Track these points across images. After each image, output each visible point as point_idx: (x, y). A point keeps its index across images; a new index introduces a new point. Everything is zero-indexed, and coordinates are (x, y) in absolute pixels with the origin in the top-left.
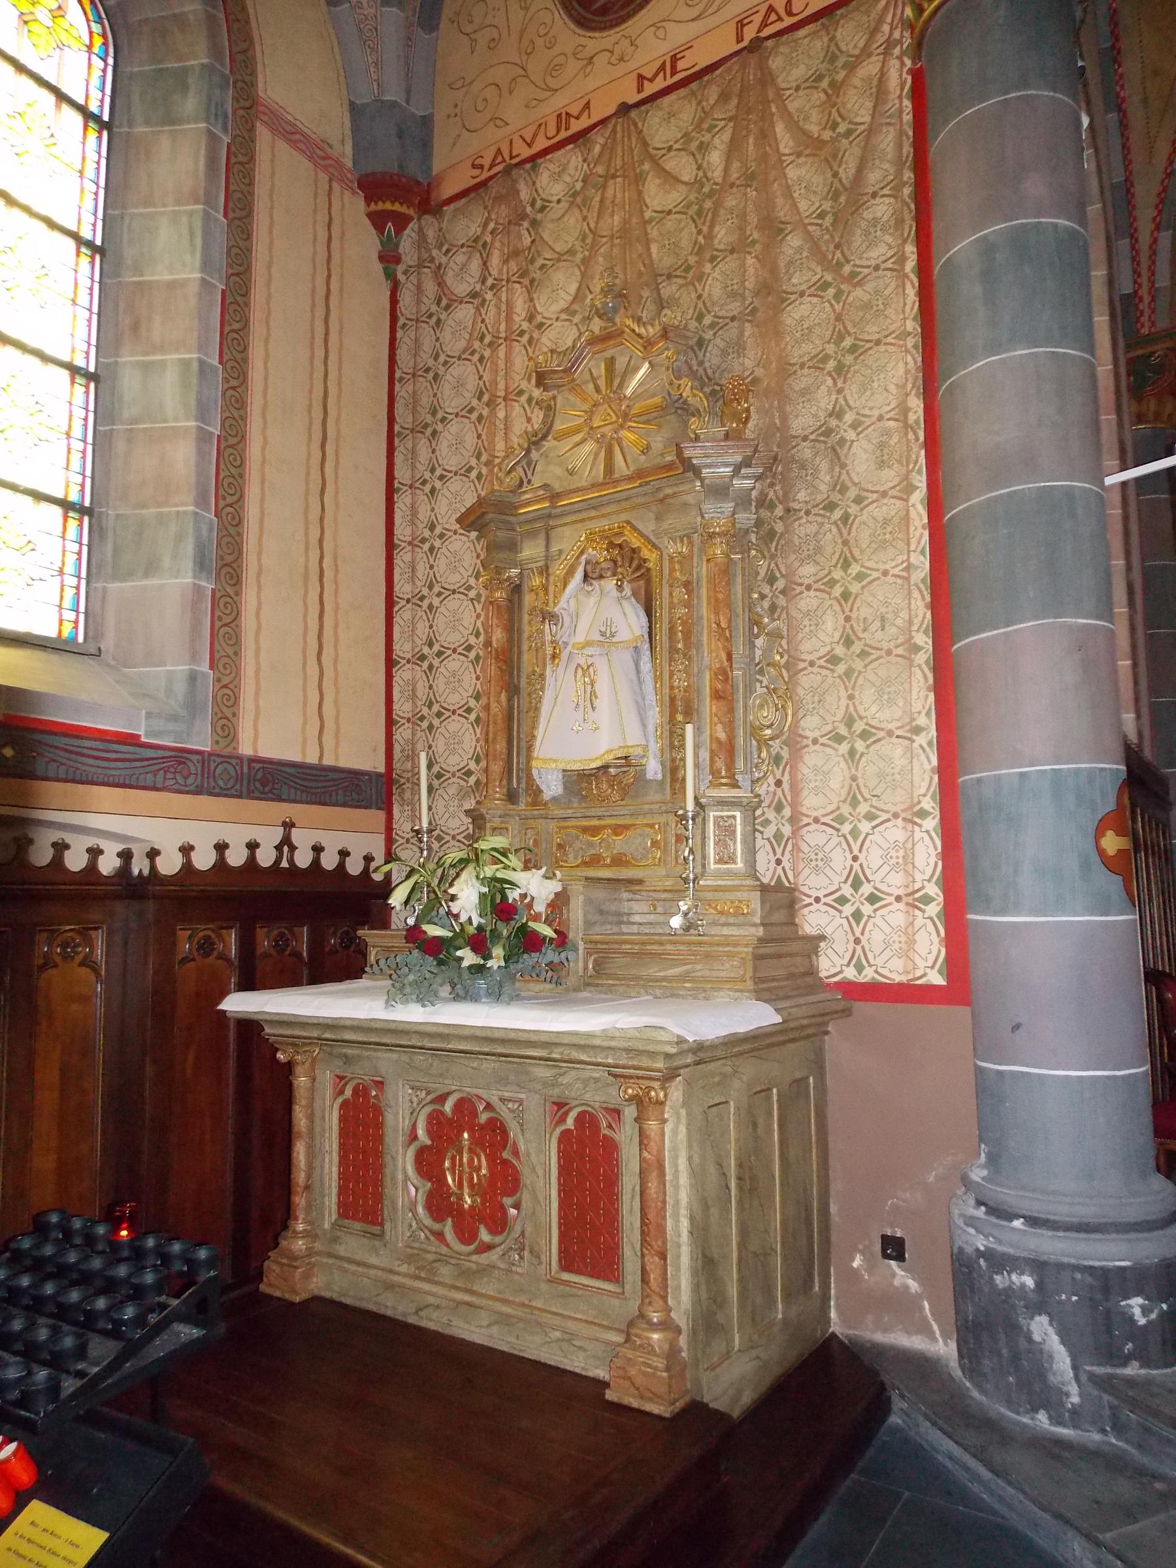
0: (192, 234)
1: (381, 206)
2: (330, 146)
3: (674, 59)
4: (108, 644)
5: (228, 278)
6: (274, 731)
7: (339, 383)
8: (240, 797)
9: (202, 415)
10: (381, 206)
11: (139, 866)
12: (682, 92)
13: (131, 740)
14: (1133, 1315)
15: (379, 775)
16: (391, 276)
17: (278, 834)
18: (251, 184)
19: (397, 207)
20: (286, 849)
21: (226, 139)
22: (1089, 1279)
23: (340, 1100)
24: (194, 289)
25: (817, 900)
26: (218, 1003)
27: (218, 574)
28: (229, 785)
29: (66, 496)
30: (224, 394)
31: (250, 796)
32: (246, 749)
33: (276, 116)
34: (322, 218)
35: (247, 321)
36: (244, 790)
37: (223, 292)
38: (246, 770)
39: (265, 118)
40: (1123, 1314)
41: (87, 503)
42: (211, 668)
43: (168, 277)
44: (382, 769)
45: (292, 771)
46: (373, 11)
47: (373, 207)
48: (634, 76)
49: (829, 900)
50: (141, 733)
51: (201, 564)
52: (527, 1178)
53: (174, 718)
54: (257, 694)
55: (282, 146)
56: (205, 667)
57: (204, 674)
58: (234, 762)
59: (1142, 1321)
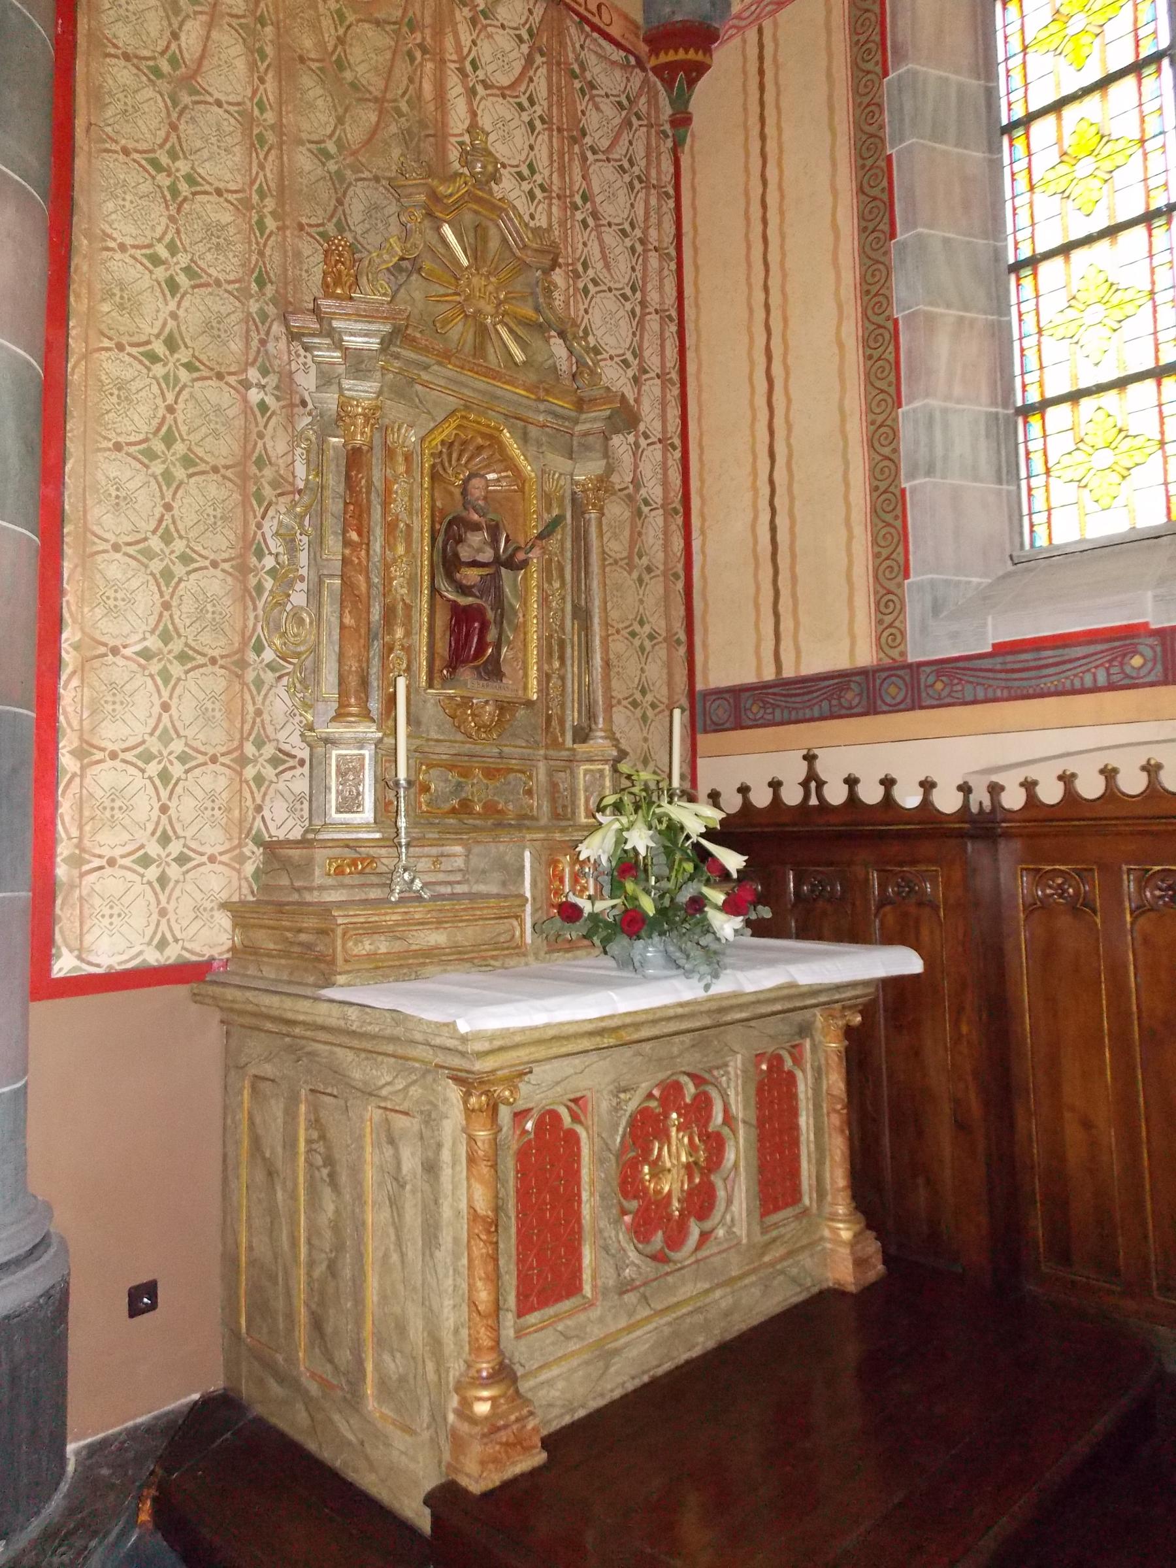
11: (980, 798)
17: (802, 769)
20: (813, 785)
23: (708, 1225)
25: (212, 859)
26: (405, 1528)
28: (898, 699)
29: (1159, 384)
44: (701, 738)
49: (199, 859)
52: (840, 1033)
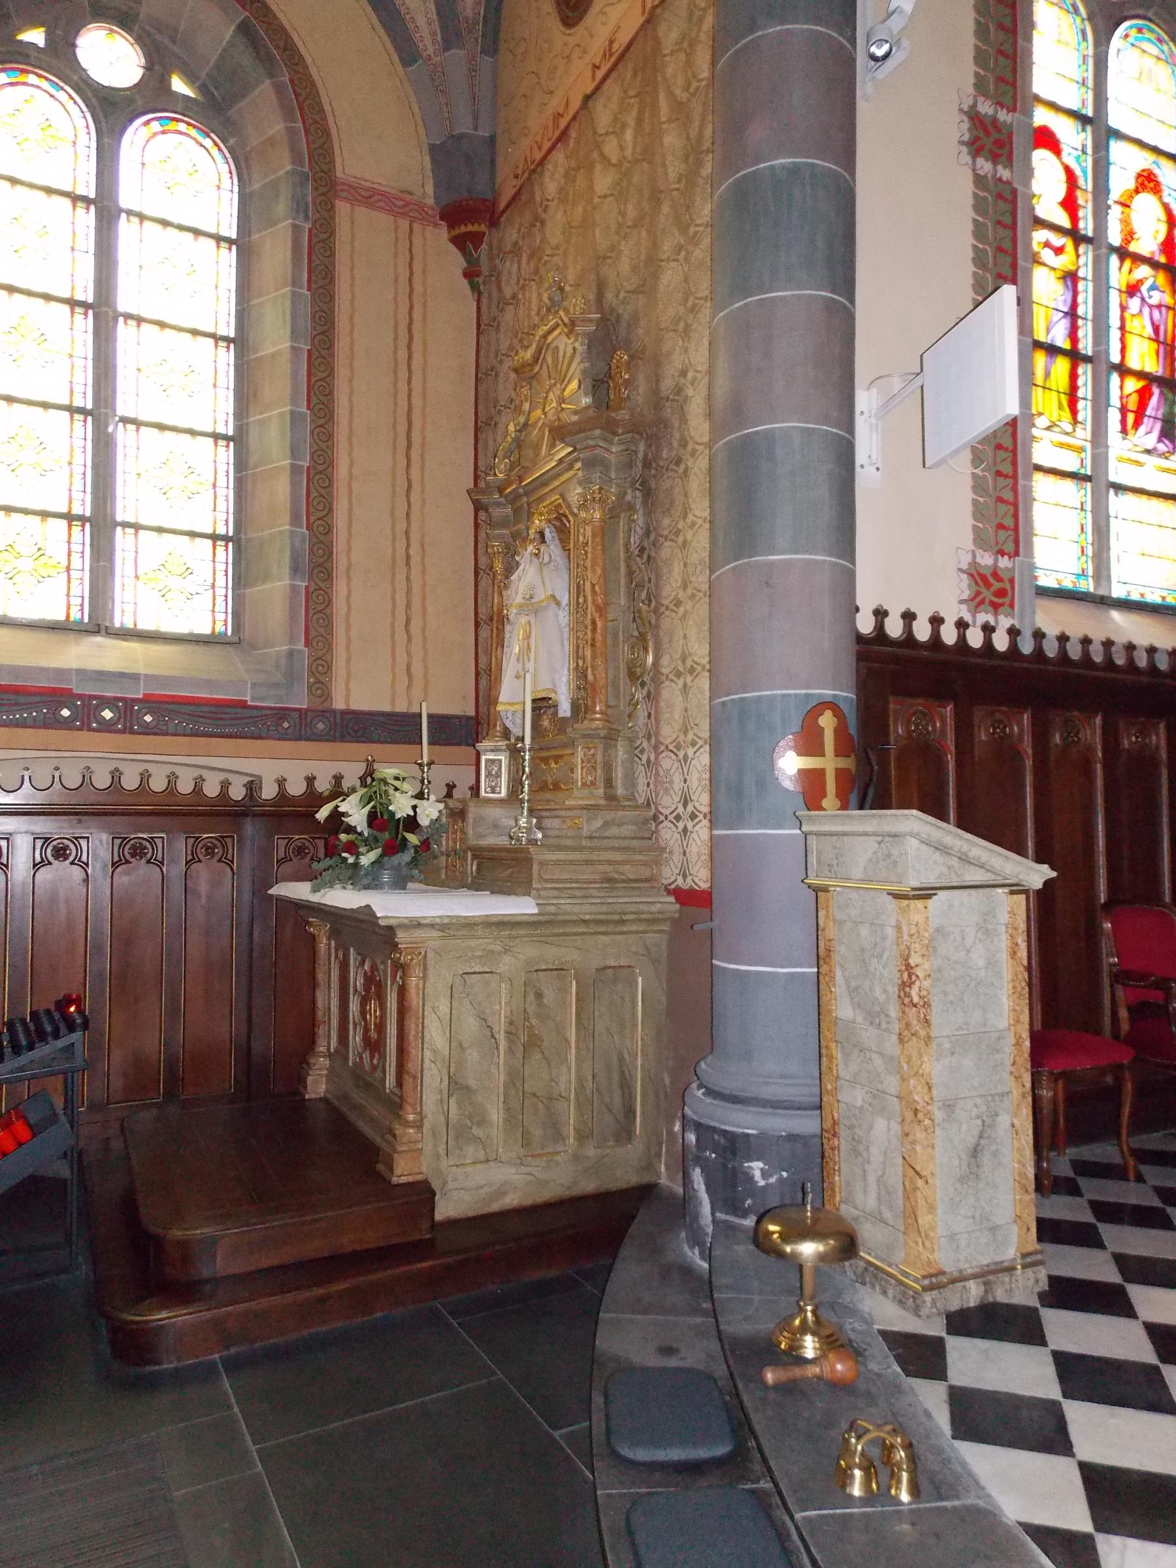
0: (284, 313)
1: (463, 229)
2: (410, 193)
3: (611, 42)
4: (246, 634)
5: (313, 339)
6: (362, 689)
7: (424, 397)
8: (334, 740)
9: (294, 452)
10: (463, 229)
12: (609, 81)
13: (243, 704)
14: (753, 1177)
15: (469, 718)
16: (475, 288)
17: (361, 768)
18: (332, 254)
19: (470, 228)
21: (308, 226)
22: (723, 1141)
24: (287, 355)
27: (311, 573)
30: (312, 432)
31: (343, 739)
32: (339, 704)
33: (354, 188)
34: (404, 258)
35: (332, 369)
36: (337, 734)
37: (309, 351)
38: (338, 721)
39: (343, 194)
40: (746, 1174)
41: (231, 534)
42: (306, 646)
43: (271, 351)
44: (472, 713)
45: (381, 719)
46: (439, 59)
47: (457, 231)
48: (590, 66)
50: (248, 698)
51: (295, 570)
53: (276, 685)
54: (348, 661)
55: (362, 212)
56: (301, 646)
57: (299, 651)
58: (328, 715)
59: (762, 1183)
